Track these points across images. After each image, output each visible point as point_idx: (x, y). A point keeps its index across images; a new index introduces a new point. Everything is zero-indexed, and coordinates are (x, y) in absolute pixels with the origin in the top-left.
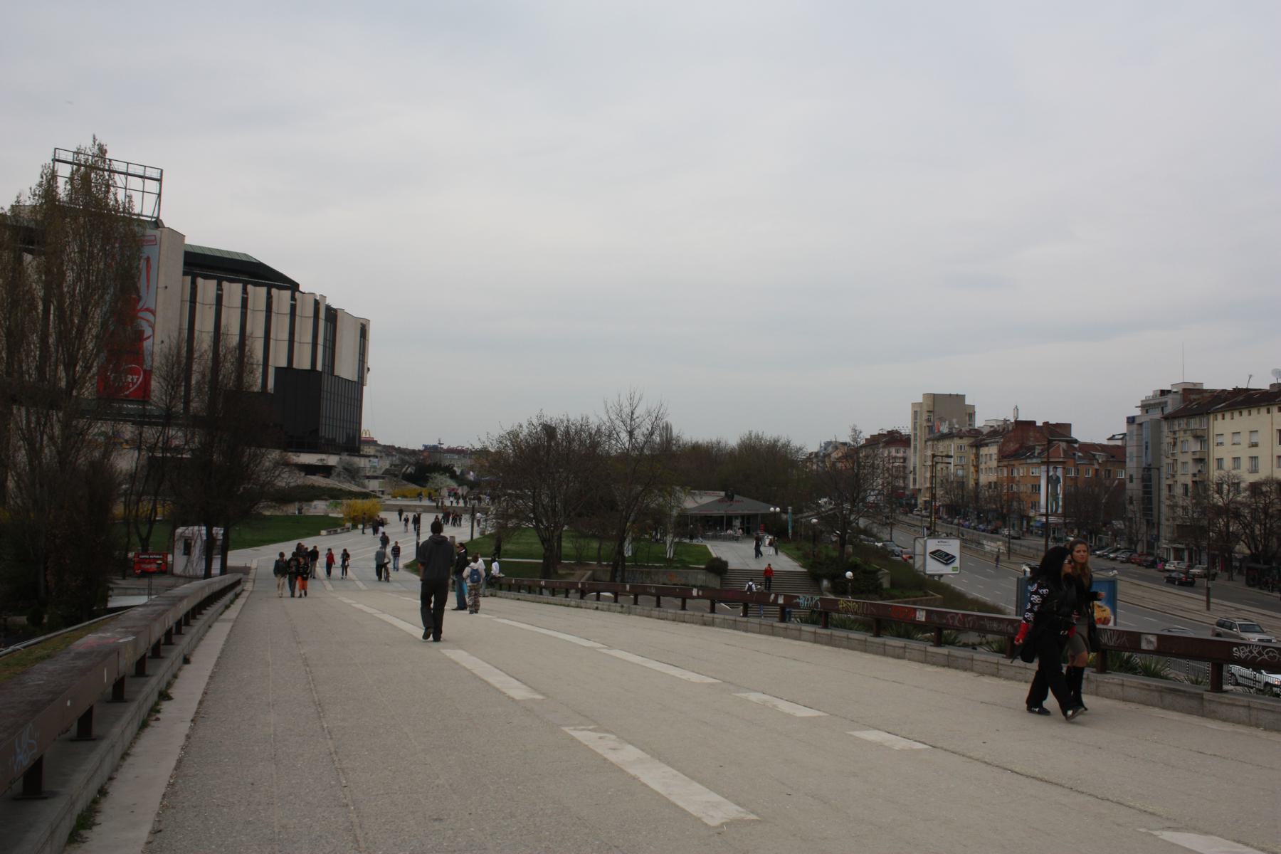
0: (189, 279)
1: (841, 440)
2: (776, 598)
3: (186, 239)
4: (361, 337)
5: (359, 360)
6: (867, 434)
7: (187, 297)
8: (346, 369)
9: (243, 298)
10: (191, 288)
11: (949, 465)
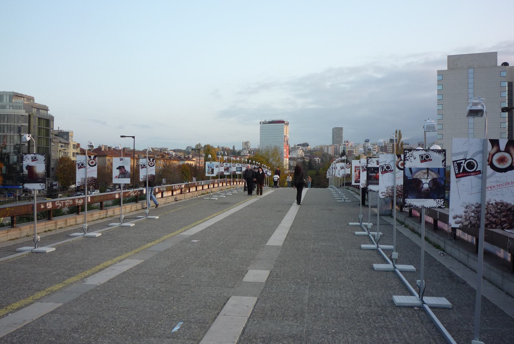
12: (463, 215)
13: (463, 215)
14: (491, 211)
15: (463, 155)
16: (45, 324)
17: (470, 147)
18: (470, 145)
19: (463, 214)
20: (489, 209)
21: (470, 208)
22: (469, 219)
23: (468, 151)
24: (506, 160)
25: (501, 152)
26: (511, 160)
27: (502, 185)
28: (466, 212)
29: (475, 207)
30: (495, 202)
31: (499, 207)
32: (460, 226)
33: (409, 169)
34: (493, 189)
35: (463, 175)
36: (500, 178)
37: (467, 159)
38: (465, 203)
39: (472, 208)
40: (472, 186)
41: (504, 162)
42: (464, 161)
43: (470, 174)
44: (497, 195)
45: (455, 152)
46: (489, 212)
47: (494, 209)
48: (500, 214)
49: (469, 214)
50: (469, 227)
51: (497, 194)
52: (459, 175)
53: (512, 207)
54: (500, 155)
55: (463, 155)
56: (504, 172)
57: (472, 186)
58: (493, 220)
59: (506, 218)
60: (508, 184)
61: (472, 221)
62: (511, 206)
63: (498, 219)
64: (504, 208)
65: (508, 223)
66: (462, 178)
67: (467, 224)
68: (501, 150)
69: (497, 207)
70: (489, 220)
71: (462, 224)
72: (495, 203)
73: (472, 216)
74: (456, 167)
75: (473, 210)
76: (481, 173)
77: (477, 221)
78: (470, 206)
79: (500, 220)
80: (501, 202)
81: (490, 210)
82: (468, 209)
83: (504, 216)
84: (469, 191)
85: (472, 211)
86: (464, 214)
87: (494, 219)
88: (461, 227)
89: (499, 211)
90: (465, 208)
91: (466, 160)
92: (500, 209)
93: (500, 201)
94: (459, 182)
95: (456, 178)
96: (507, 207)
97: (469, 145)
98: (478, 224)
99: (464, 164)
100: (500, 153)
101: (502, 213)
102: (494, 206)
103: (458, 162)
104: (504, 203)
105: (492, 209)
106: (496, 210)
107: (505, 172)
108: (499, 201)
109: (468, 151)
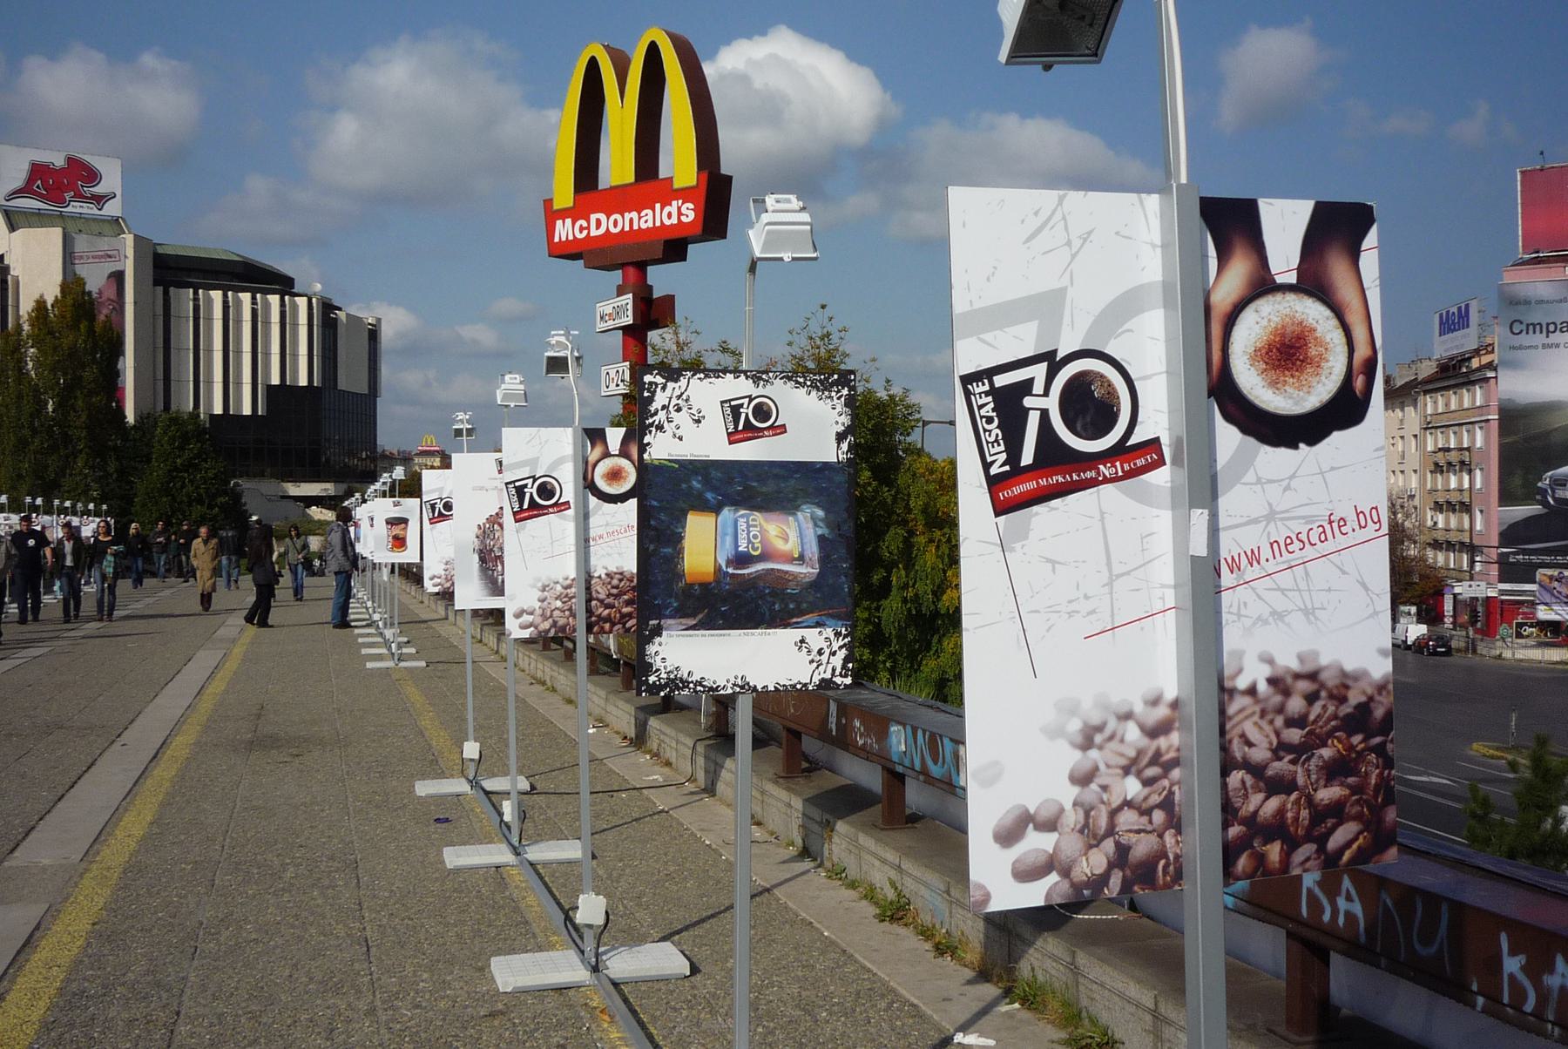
0: (160, 289)
1: (935, 456)
2: (943, 621)
3: (582, 265)
4: (370, 339)
5: (369, 368)
6: (803, 390)
7: (160, 310)
8: (351, 379)
9: (253, 308)
10: (164, 300)
11: (455, 668)
12: (1068, 806)
13: (1068, 806)
14: (1250, 744)
15: (528, 468)
16: (691, 330)
17: (1074, 256)
18: (1076, 243)
19: (1067, 794)
20: (1237, 731)
21: (1111, 738)
22: (551, 616)
23: (1061, 293)
24: (1313, 352)
25: (1279, 296)
26: (1345, 349)
27: (1303, 537)
28: (1083, 779)
29: (1142, 728)
30: (605, 571)
31: (615, 582)
32: (1048, 896)
33: (1054, 348)
34: (1251, 573)
35: (1043, 482)
36: (1287, 488)
37: (1060, 355)
38: (1072, 709)
39: (1122, 741)
40: (1109, 564)
41: (1300, 369)
42: (1039, 372)
43: (1092, 474)
44: (1278, 616)
45: (976, 306)
46: (1238, 755)
47: (1264, 724)
48: (1308, 759)
49: (1105, 788)
50: (1117, 889)
51: (1274, 613)
52: (522, 516)
53: (1371, 699)
54: (611, 465)
55: (528, 468)
56: (622, 502)
57: (1109, 564)
58: (1261, 813)
59: (1342, 784)
60: (1335, 525)
61: (1134, 838)
62: (1369, 691)
63: (1294, 796)
64: (1324, 707)
65: (1358, 818)
66: (1035, 508)
67: (1098, 872)
68: (1279, 280)
69: (610, 583)
70: (1243, 813)
71: (536, 628)
72: (606, 574)
73: (1128, 804)
74: (990, 420)
75: (1132, 753)
76: (1161, 462)
77: (1161, 836)
78: (552, 585)
79: (620, 612)
80: (620, 571)
81: (1243, 736)
82: (1100, 748)
83: (1334, 771)
84: (1093, 612)
85: (1123, 762)
86: (1075, 790)
87: (607, 611)
88: (533, 636)
89: (615, 591)
90: (1075, 745)
91: (1054, 363)
92: (616, 587)
93: (1301, 659)
94: (1018, 546)
95: (997, 514)
96: (1343, 700)
97: (1069, 243)
98: (1171, 857)
99: (1046, 393)
100: (1270, 298)
101: (1318, 752)
102: (1266, 699)
103: (517, 484)
104: (1324, 676)
105: (1256, 724)
106: (1278, 734)
107: (1313, 441)
108: (1295, 665)
109: (1061, 293)
